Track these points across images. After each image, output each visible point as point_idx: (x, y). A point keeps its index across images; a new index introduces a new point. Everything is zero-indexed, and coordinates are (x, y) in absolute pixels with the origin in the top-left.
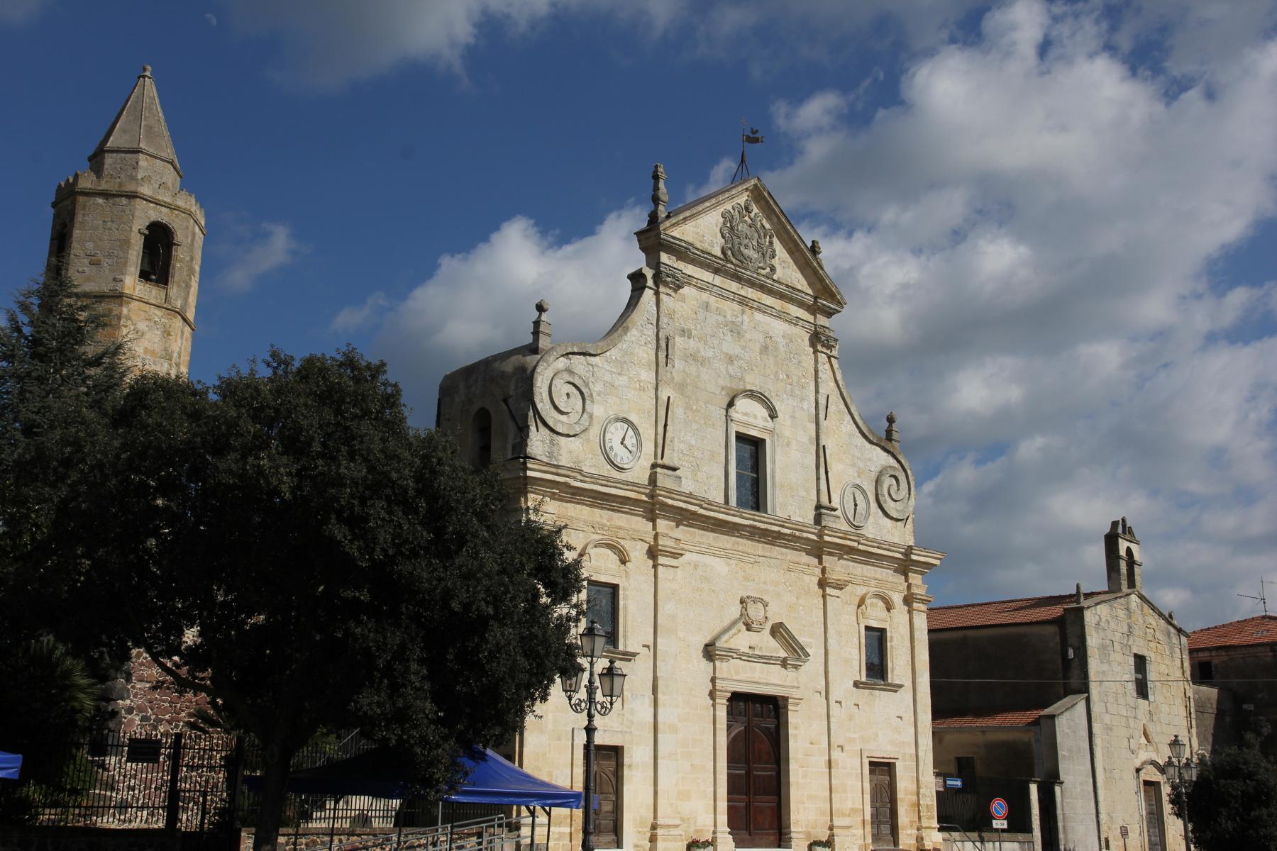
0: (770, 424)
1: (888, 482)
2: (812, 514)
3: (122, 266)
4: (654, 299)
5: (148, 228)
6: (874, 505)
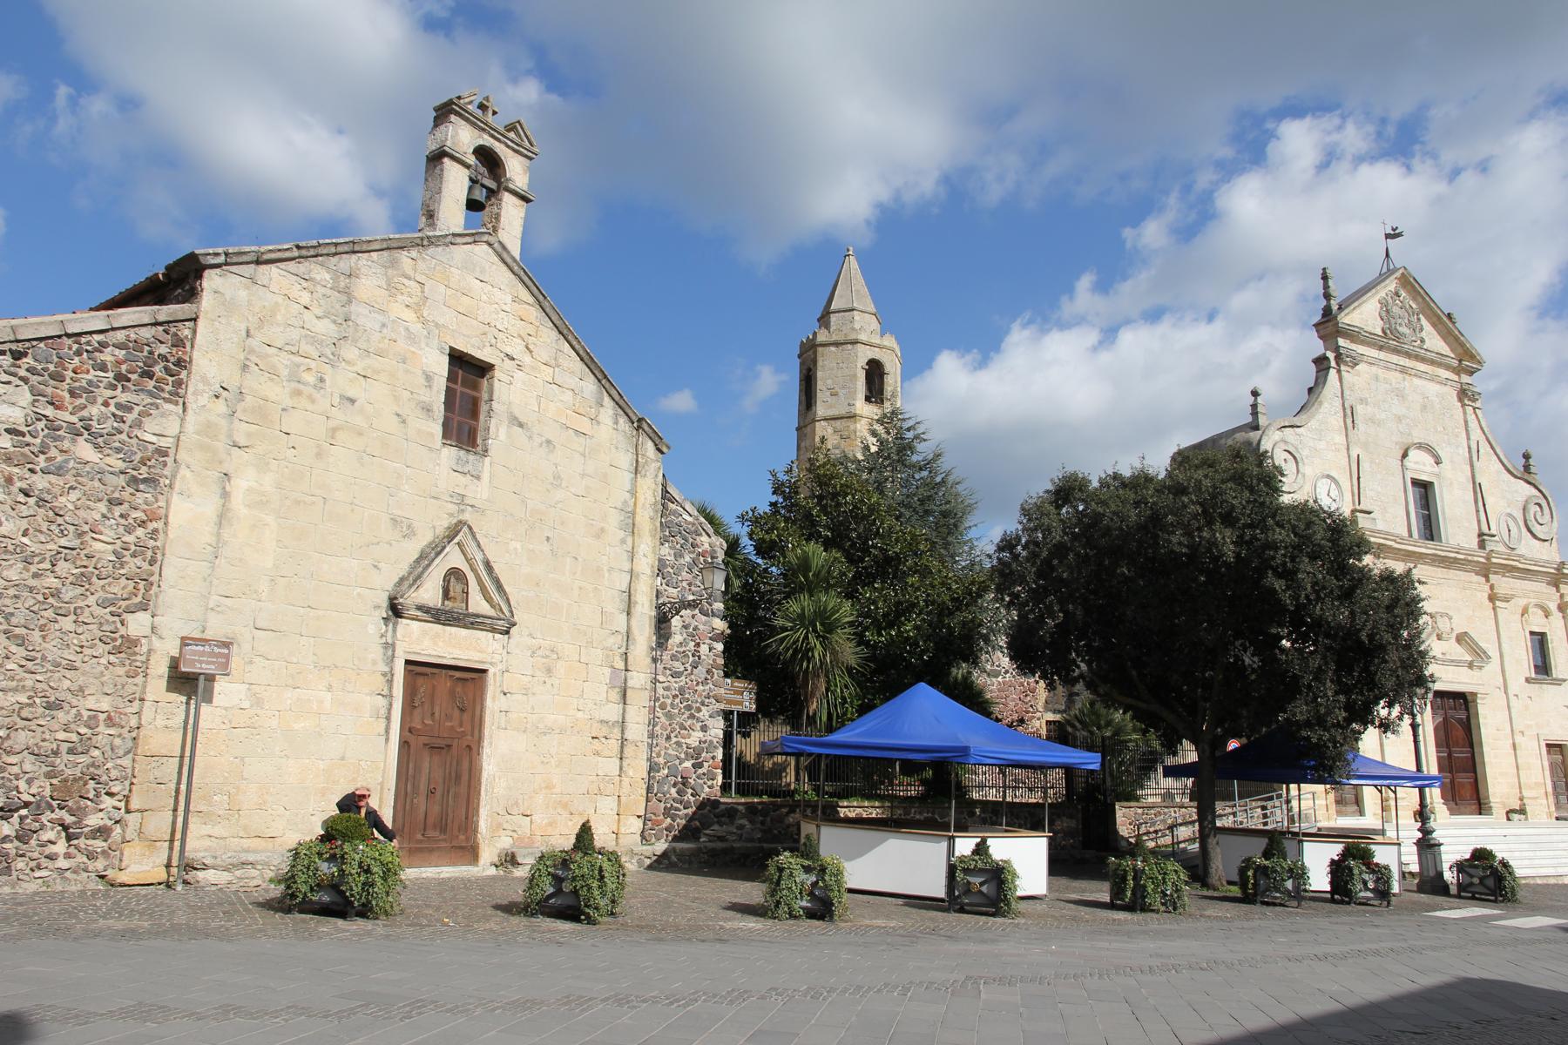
0: (1436, 469)
1: (1533, 509)
2: (1476, 540)
6: (1524, 530)
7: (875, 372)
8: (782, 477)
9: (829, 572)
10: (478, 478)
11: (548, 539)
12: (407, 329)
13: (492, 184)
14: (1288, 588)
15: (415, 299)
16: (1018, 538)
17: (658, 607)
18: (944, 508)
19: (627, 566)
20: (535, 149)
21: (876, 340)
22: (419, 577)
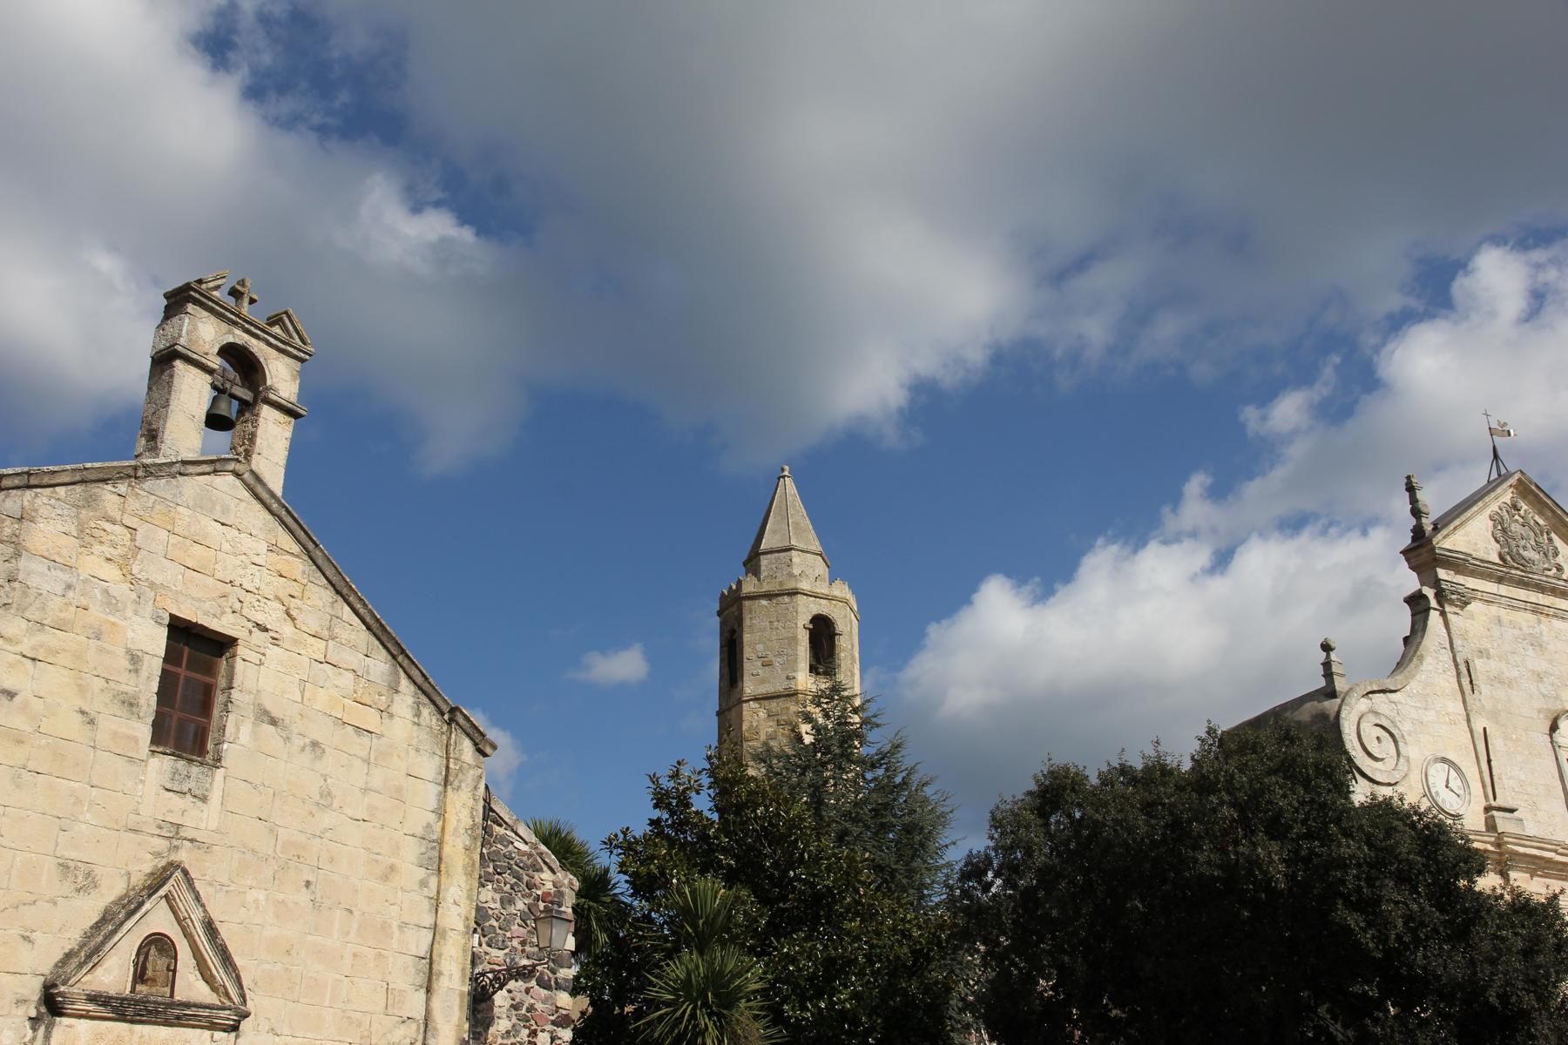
3: (792, 664)
4: (1441, 620)
5: (812, 621)
7: (822, 633)
8: (666, 784)
9: (729, 917)
10: (204, 799)
11: (308, 884)
12: (106, 591)
13: (246, 394)
14: (1369, 925)
15: (121, 550)
16: (988, 861)
17: (474, 979)
18: (907, 819)
19: (428, 920)
20: (310, 349)
21: (823, 589)
22: (97, 950)
